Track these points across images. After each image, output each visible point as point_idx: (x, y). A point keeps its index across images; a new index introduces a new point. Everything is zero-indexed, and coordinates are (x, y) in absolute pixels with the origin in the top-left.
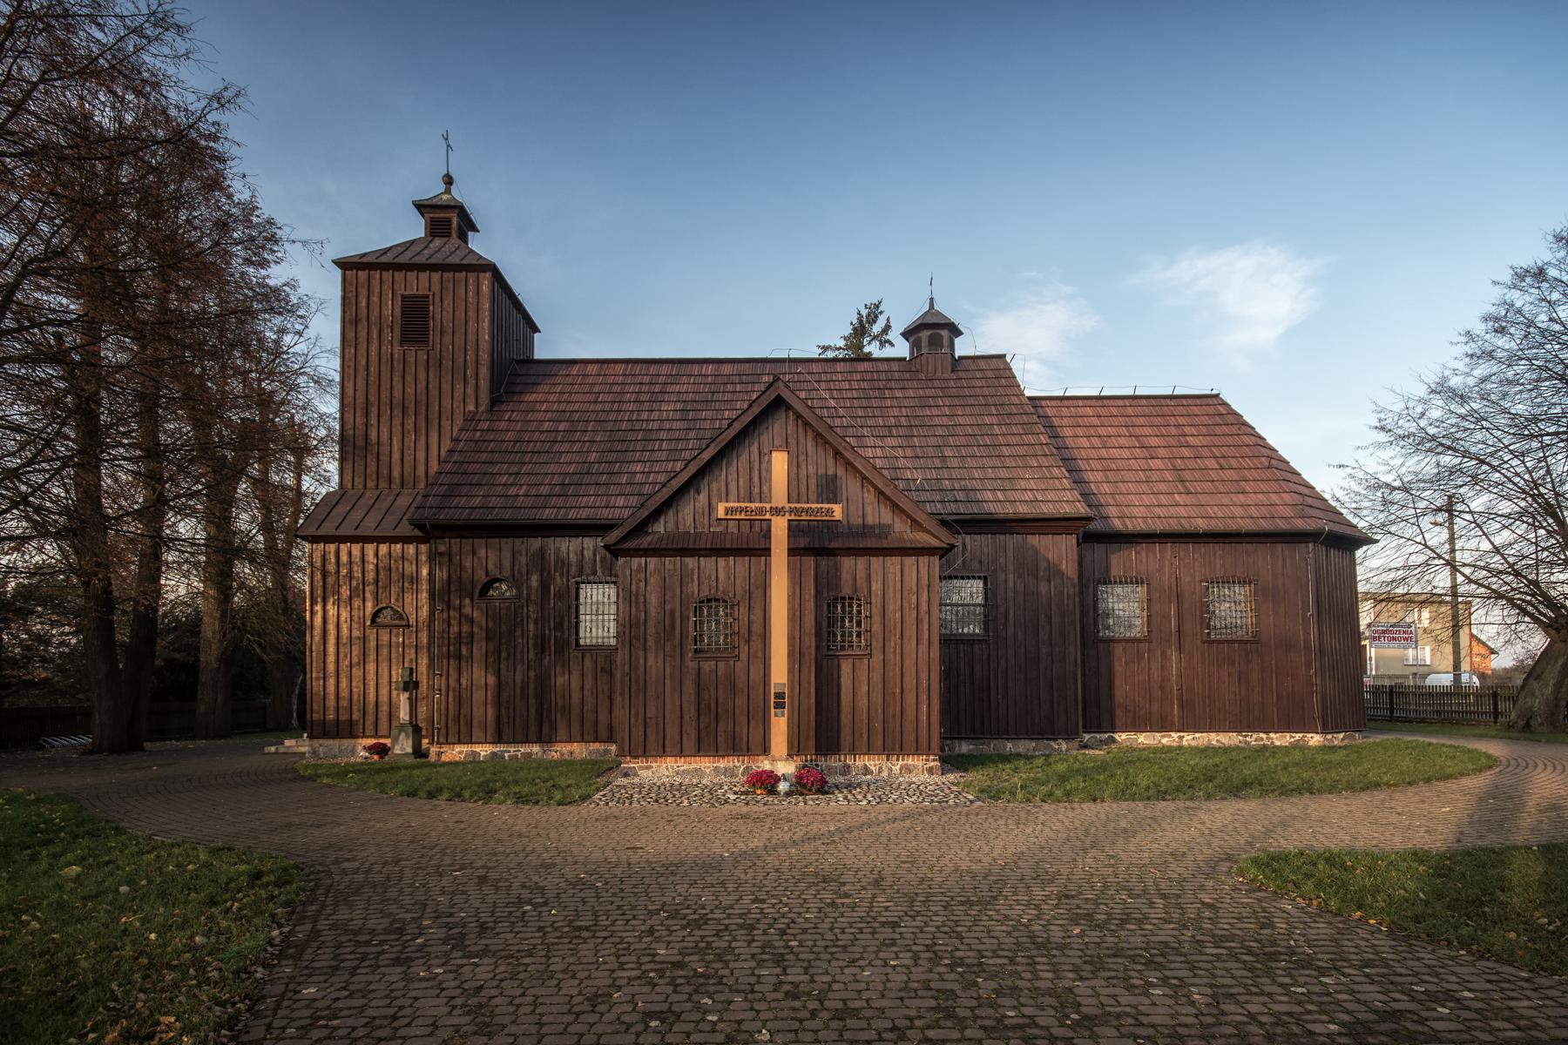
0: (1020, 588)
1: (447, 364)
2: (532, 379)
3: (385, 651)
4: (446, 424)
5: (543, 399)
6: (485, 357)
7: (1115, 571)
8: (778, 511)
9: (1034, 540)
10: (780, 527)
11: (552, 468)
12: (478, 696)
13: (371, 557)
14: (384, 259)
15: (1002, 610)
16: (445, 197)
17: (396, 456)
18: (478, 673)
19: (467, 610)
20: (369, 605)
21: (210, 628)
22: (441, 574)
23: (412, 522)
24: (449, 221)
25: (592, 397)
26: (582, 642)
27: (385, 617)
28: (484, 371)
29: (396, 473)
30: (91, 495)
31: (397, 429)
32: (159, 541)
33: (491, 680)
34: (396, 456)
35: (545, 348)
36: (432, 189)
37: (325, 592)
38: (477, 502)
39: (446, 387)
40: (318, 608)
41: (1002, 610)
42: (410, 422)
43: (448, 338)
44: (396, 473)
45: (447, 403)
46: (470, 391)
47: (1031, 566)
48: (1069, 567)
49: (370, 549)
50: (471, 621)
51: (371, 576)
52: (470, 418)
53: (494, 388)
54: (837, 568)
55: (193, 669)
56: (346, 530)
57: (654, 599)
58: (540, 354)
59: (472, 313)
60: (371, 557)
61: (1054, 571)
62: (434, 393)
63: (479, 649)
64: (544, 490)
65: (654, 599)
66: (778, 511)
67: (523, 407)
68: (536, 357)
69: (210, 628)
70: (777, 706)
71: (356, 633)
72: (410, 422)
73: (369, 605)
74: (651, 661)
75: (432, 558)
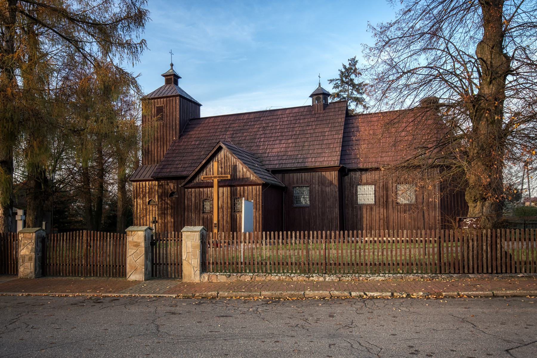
0: (320, 189)
1: (168, 126)
2: (193, 126)
3: (151, 212)
4: (168, 143)
5: (195, 133)
6: (178, 122)
7: (364, 181)
8: (215, 177)
9: (324, 173)
10: (216, 181)
11: (191, 158)
12: (169, 225)
13: (147, 186)
14: (152, 97)
15: (314, 196)
16: (171, 71)
17: (156, 154)
18: (169, 218)
19: (166, 201)
20: (147, 199)
21: (120, 204)
22: (160, 191)
23: (152, 177)
24: (171, 78)
25: (208, 131)
26: (373, 187)
27: (151, 203)
28: (178, 127)
29: (156, 159)
30: (118, 149)
31: (156, 146)
32: (142, 164)
33: (172, 220)
34: (156, 154)
35: (205, 112)
36: (166, 69)
37: (137, 196)
38: (168, 170)
39: (168, 132)
40: (135, 200)
41: (314, 196)
42: (159, 143)
43: (168, 118)
44: (156, 159)
45: (168, 138)
46: (174, 133)
47: (323, 182)
48: (336, 182)
49: (147, 183)
50: (167, 204)
51: (147, 191)
52: (175, 142)
53: (180, 132)
54: (236, 189)
55: (115, 216)
56: (141, 178)
57: (193, 199)
58: (202, 116)
59: (174, 110)
60: (147, 186)
61: (331, 183)
62: (165, 135)
63: (169, 211)
64: (186, 165)
65: (193, 199)
66: (215, 177)
67: (189, 136)
68: (201, 117)
69: (120, 204)
70: (215, 226)
71: (144, 207)
72: (159, 143)
73: (147, 199)
74: (193, 215)
75: (159, 185)
